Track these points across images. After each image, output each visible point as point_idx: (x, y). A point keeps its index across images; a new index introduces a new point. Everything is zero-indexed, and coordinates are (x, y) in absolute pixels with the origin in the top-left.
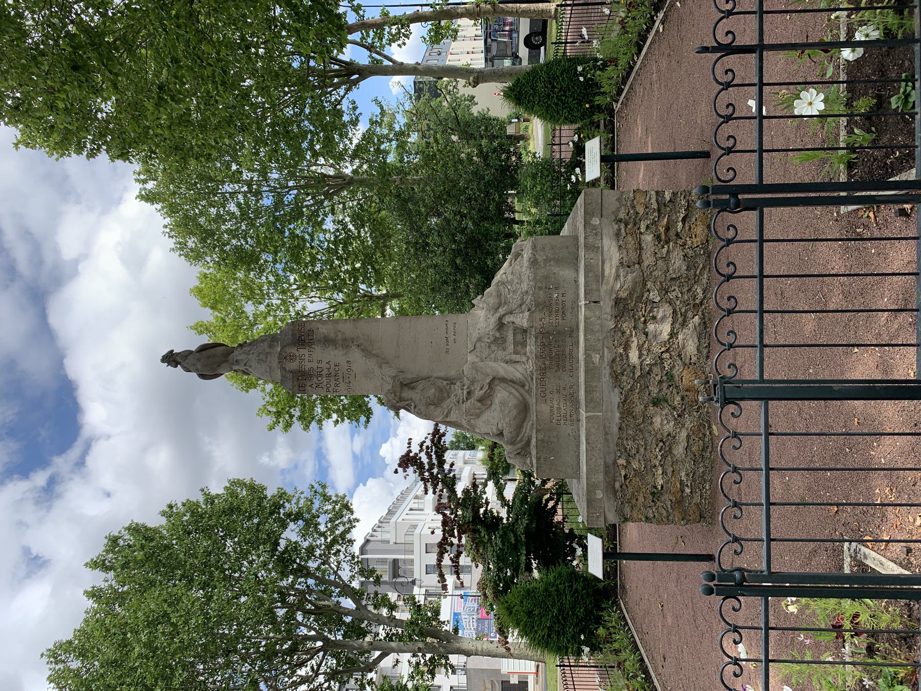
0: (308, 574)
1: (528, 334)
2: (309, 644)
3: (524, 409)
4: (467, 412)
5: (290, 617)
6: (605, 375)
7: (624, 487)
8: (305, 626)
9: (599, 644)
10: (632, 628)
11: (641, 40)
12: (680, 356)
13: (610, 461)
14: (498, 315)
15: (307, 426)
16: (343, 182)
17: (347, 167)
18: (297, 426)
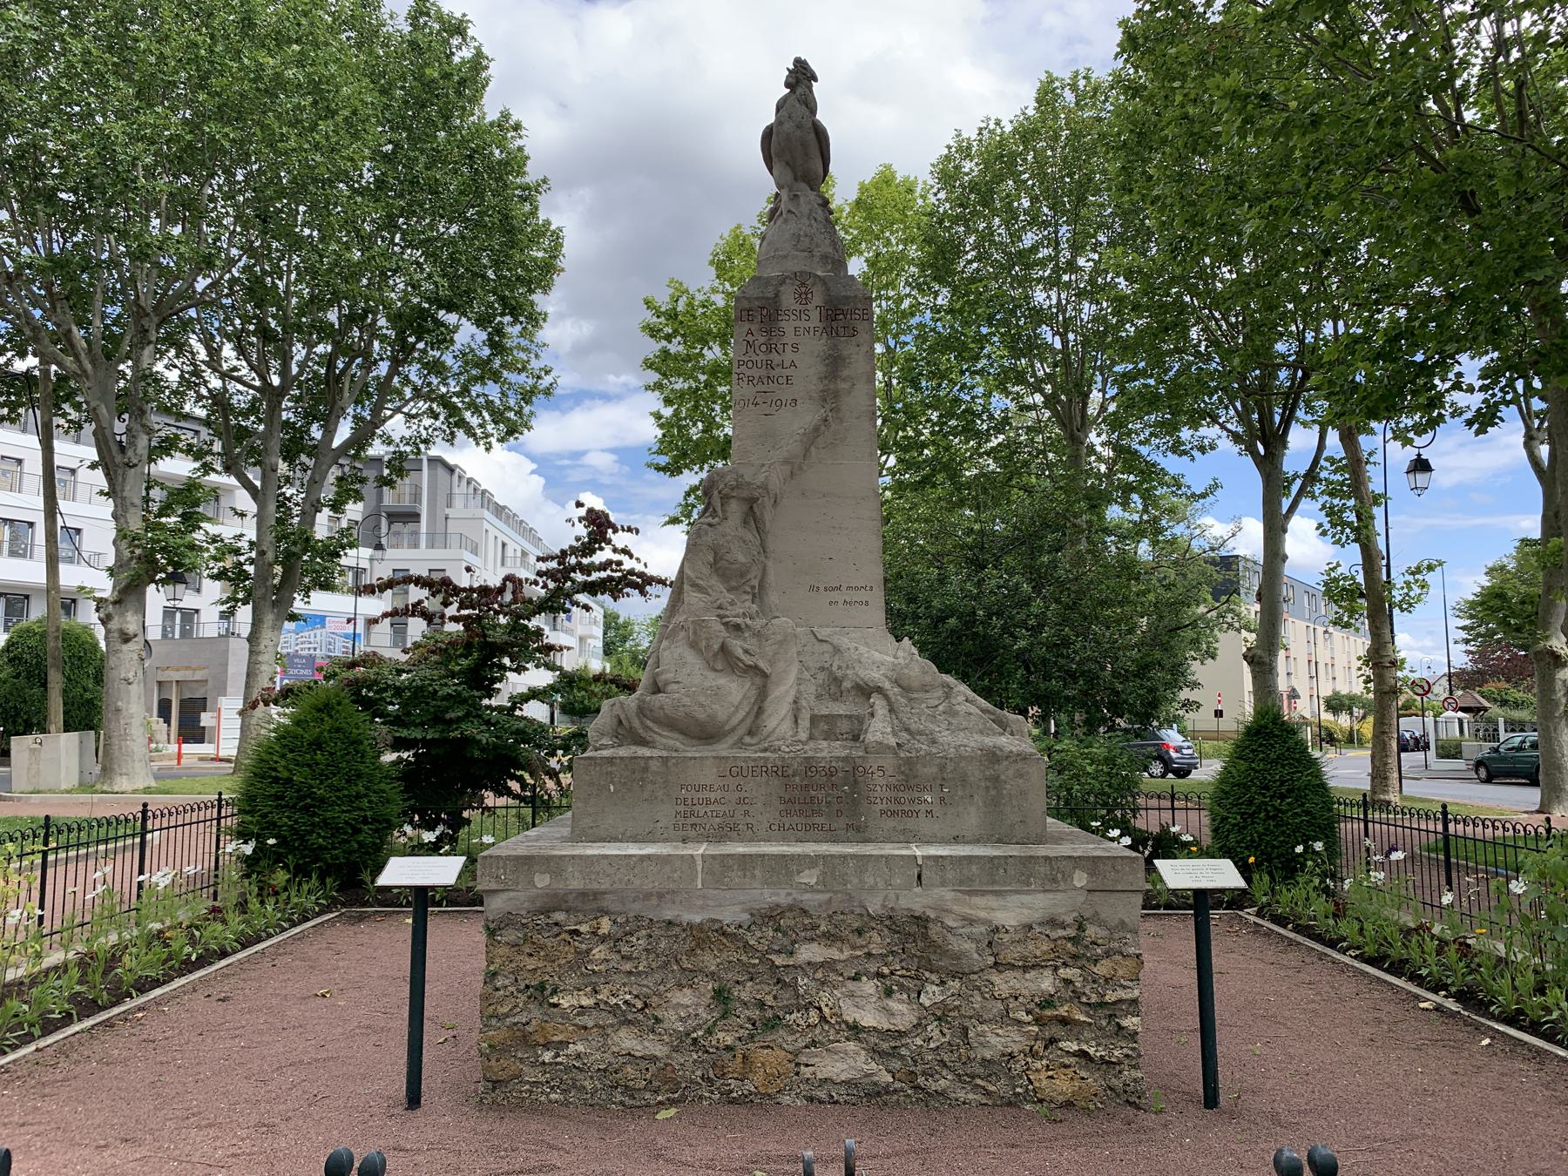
0: (396, 363)
1: (850, 744)
2: (275, 364)
3: (706, 733)
4: (700, 624)
5: (325, 331)
6: (778, 894)
7: (556, 929)
8: (307, 358)
9: (259, 873)
10: (286, 935)
11: (1392, 964)
12: (814, 1043)
13: (608, 901)
14: (887, 685)
15: (652, 364)
16: (1073, 423)
17: (1099, 435)
18: (653, 347)
